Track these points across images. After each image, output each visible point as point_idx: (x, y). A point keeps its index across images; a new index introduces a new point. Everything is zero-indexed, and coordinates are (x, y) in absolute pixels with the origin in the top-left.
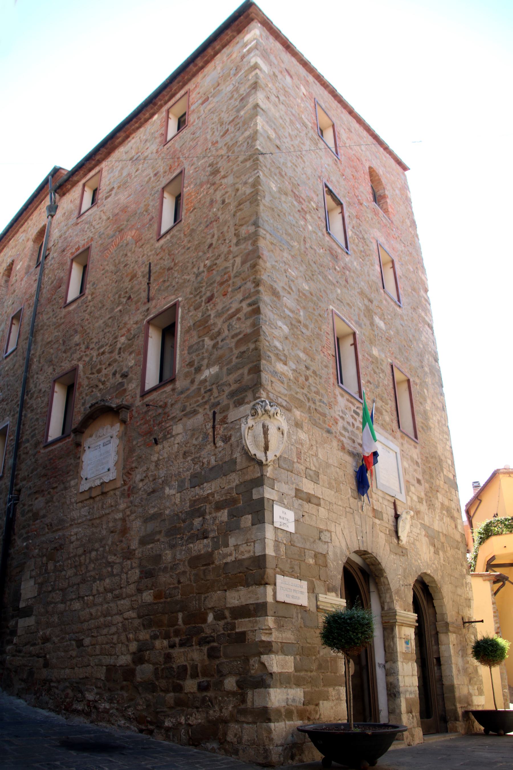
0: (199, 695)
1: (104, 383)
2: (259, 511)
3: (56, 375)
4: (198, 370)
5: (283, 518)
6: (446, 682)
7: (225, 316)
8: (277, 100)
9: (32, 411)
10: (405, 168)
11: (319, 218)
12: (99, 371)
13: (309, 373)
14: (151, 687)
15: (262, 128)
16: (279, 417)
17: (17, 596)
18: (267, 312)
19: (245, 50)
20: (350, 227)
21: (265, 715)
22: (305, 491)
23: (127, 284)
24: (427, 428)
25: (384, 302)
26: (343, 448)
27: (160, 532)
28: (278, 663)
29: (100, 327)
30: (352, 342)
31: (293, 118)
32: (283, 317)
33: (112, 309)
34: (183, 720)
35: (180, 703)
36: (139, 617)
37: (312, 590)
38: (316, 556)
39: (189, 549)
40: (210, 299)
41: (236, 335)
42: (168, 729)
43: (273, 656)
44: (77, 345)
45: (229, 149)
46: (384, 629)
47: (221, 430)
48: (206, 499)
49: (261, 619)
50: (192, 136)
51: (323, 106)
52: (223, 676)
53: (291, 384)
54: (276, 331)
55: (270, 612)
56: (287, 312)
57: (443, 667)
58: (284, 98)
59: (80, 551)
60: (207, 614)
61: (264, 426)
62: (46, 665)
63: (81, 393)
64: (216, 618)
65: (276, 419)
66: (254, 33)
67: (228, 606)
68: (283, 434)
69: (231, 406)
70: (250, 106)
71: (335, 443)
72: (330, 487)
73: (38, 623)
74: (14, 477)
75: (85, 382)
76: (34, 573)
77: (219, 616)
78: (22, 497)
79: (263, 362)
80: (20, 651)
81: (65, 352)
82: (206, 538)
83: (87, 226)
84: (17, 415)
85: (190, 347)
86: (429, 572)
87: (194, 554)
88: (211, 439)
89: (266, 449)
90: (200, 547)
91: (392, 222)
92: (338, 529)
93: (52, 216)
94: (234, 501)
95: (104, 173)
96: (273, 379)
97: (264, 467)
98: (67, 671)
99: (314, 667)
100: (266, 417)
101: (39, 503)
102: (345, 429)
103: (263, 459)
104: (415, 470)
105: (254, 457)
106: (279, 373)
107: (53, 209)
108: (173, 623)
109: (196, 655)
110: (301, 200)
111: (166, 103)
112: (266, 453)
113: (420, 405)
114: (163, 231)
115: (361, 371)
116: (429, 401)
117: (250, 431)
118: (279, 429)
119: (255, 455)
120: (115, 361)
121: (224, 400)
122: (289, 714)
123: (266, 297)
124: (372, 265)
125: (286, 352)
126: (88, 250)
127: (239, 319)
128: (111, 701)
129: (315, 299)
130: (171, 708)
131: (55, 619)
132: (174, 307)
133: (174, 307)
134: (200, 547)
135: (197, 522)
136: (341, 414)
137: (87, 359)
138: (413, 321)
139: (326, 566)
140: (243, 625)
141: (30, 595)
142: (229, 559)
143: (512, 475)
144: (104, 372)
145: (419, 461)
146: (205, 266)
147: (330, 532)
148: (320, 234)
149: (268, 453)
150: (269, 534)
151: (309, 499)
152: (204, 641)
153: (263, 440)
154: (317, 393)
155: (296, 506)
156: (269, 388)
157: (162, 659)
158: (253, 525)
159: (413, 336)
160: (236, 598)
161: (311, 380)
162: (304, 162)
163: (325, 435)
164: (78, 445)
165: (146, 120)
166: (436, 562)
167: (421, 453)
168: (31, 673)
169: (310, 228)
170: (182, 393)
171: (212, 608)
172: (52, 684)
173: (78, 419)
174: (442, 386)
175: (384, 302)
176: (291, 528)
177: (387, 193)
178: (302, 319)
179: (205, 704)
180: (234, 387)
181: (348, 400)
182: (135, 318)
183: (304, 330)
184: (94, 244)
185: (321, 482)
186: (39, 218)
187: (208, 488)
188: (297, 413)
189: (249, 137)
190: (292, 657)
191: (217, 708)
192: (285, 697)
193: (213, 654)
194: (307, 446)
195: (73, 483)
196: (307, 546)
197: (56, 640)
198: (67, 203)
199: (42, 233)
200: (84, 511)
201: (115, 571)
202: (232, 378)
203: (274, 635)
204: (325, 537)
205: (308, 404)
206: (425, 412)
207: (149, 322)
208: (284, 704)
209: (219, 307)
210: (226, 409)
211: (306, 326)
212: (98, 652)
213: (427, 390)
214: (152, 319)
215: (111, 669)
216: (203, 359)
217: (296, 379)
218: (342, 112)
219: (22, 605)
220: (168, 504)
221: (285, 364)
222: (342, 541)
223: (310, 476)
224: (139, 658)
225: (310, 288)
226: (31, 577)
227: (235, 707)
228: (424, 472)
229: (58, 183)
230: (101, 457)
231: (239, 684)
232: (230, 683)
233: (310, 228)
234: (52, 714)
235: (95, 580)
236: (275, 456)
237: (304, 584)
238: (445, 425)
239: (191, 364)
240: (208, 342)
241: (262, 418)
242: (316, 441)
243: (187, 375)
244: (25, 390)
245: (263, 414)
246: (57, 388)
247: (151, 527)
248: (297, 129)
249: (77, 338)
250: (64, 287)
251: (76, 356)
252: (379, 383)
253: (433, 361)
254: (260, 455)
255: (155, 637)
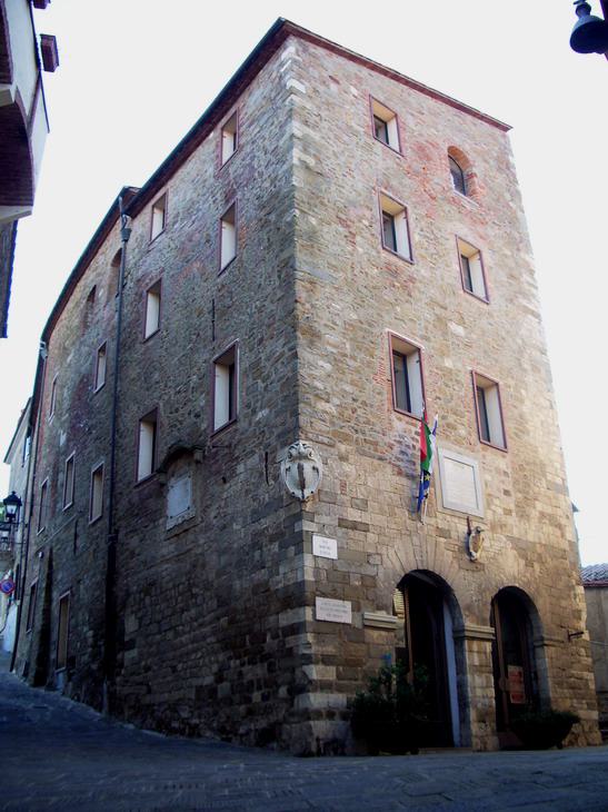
0: (263, 704)
1: (181, 423)
2: (299, 542)
3: (141, 415)
4: (254, 412)
5: (324, 547)
6: (543, 696)
7: (273, 360)
8: (317, 119)
9: (123, 451)
10: (505, 128)
11: (373, 235)
12: (177, 410)
13: (355, 405)
14: (229, 702)
15: (299, 159)
17: (123, 633)
18: (305, 354)
19: (282, 70)
20: (418, 230)
21: (307, 715)
22: (350, 519)
23: (195, 321)
24: (522, 431)
25: (464, 303)
26: (400, 473)
27: (231, 565)
28: (315, 672)
29: (175, 365)
30: (417, 359)
31: (338, 132)
32: (326, 356)
33: (185, 346)
34: (252, 726)
35: (250, 712)
36: (218, 641)
37: (356, 608)
38: (363, 578)
39: (252, 580)
40: (261, 341)
41: (281, 378)
42: (242, 735)
43: (312, 666)
44: (157, 383)
45: (272, 182)
46: (456, 644)
47: (271, 470)
48: (261, 533)
49: (302, 636)
51: (382, 99)
52: (279, 686)
53: (335, 420)
54: (315, 367)
55: (309, 628)
56: (330, 349)
57: (539, 682)
58: (327, 113)
59: (171, 585)
60: (265, 635)
62: (149, 691)
63: (163, 432)
64: (273, 638)
66: (291, 49)
67: (281, 626)
69: (279, 447)
70: (287, 136)
71: (389, 469)
72: (382, 512)
73: (141, 654)
74: (111, 516)
75: (166, 422)
76: (134, 609)
77: (275, 637)
78: (121, 536)
79: (301, 405)
80: (127, 681)
81: (148, 389)
82: (264, 567)
83: (158, 254)
84: (110, 455)
85: (248, 388)
86: (517, 585)
87: (255, 583)
88: (264, 477)
90: (262, 575)
91: (481, 205)
92: (391, 552)
93: (126, 241)
94: (283, 534)
95: (170, 196)
96: (313, 420)
98: (166, 695)
99: (360, 676)
101: (134, 541)
102: (402, 452)
104: (503, 482)
106: (319, 414)
107: (126, 234)
108: (244, 645)
109: (260, 671)
110: (349, 223)
111: (219, 120)
113: (513, 409)
114: (223, 266)
115: (426, 388)
116: (527, 402)
120: (190, 400)
121: (273, 441)
122: (330, 714)
123: (302, 340)
124: (447, 266)
125: (329, 390)
126: (159, 282)
127: (283, 363)
128: (200, 717)
129: (365, 326)
130: (243, 718)
131: (154, 649)
132: (233, 348)
133: (233, 348)
134: (262, 575)
135: (257, 553)
136: (398, 439)
137: (166, 397)
138: (507, 315)
139: (375, 586)
140: (291, 641)
141: (132, 629)
142: (280, 585)
144: (181, 411)
145: (509, 471)
146: (256, 307)
147: (381, 555)
148: (374, 253)
150: (308, 562)
151: (354, 526)
152: (264, 658)
154: (368, 422)
155: (340, 534)
156: (309, 429)
157: (236, 677)
158: (296, 554)
159: (508, 332)
160: (285, 619)
161: (359, 412)
162: (354, 177)
163: (376, 462)
164: (163, 485)
165: (204, 138)
166: (528, 575)
167: (512, 462)
168: (138, 700)
169: (360, 250)
170: (242, 434)
171: (269, 629)
172: (156, 708)
173: (162, 457)
174: (551, 381)
175: (464, 303)
176: (334, 555)
177: (475, 170)
178: (348, 352)
179: (267, 711)
180: (280, 429)
181: (407, 423)
182: (204, 357)
183: (351, 363)
184: (165, 275)
185: (370, 509)
186: (114, 243)
187: (266, 522)
188: (343, 447)
189: (287, 171)
190: (334, 668)
191: (275, 713)
192: (326, 701)
193: (270, 670)
194: (354, 477)
195: (161, 521)
196: (353, 569)
197: (155, 668)
198: (139, 226)
199: (119, 257)
200: (172, 548)
201: (198, 602)
202: (279, 420)
203: (313, 648)
204: (375, 560)
205: (355, 436)
206: (521, 416)
207: (215, 362)
208: (325, 706)
209: (268, 350)
210: (274, 451)
211: (353, 358)
212: (188, 675)
213: (526, 389)
214: (217, 359)
215: (199, 689)
216: (257, 401)
217: (341, 414)
218: (409, 95)
219: (126, 639)
220: (236, 538)
221: (328, 401)
222: (398, 558)
223: (357, 505)
224: (220, 679)
225: (358, 315)
226: (132, 612)
227: (287, 711)
228: (516, 482)
229: (131, 203)
230: (179, 500)
231: (289, 691)
232: (283, 691)
233: (360, 250)
234: (156, 734)
235: (183, 611)
237: (348, 605)
238: (553, 424)
239: (248, 406)
240: (261, 384)
242: (365, 471)
243: (246, 416)
244: (115, 430)
246: (142, 427)
247: (224, 559)
248: (344, 143)
249: (156, 376)
250: (142, 319)
251: (156, 394)
252: (452, 396)
253: (539, 353)
254: (298, 493)
255: (230, 658)
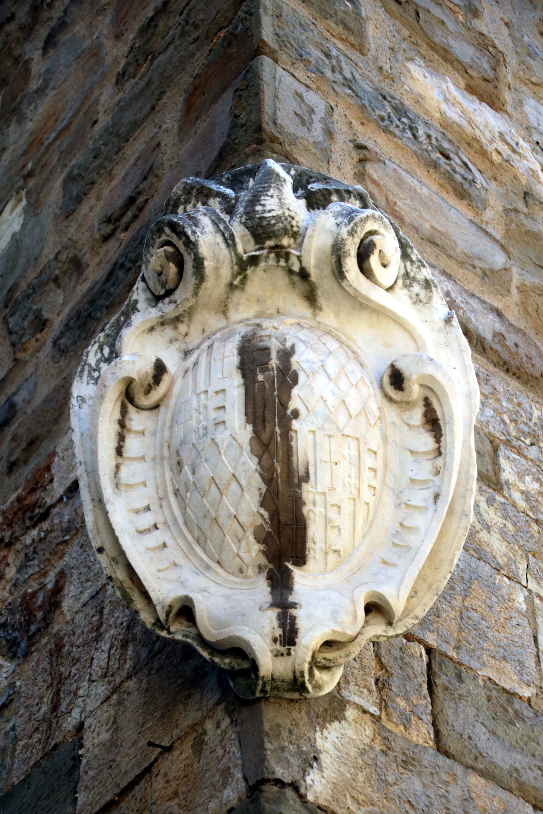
16: (385, 282)
50: (219, 731)
61: (252, 357)
65: (360, 304)
68: (433, 423)
89: (284, 542)
97: (271, 715)
100: (267, 284)
103: (259, 634)
105: (178, 631)
112: (280, 583)
117: (138, 420)
118: (397, 379)
119: (186, 611)
143: (542, 92)
149: (302, 580)
153: (249, 465)
236: (375, 608)
241: (243, 312)
245: (245, 265)
254: (230, 604)
